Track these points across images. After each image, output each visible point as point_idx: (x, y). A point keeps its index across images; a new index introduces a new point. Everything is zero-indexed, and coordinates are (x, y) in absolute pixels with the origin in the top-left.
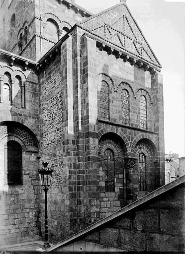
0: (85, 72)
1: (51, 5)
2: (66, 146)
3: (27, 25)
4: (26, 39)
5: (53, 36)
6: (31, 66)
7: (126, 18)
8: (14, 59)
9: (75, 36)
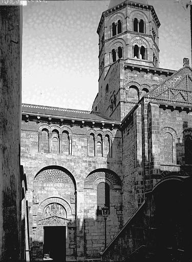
0: (150, 130)
1: (133, 76)
2: (137, 186)
3: (115, 93)
4: (115, 103)
5: (134, 98)
6: (116, 126)
7: (189, 77)
8: (103, 124)
9: (143, 105)
